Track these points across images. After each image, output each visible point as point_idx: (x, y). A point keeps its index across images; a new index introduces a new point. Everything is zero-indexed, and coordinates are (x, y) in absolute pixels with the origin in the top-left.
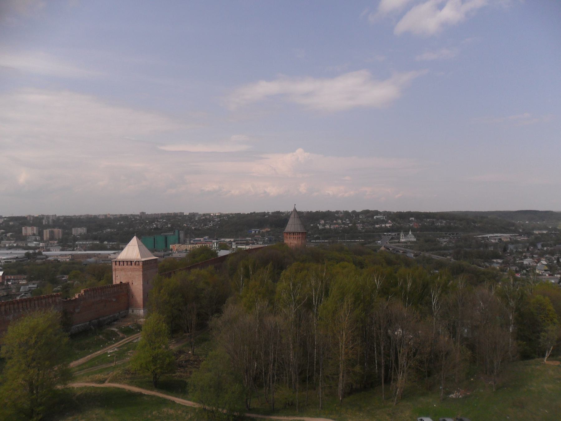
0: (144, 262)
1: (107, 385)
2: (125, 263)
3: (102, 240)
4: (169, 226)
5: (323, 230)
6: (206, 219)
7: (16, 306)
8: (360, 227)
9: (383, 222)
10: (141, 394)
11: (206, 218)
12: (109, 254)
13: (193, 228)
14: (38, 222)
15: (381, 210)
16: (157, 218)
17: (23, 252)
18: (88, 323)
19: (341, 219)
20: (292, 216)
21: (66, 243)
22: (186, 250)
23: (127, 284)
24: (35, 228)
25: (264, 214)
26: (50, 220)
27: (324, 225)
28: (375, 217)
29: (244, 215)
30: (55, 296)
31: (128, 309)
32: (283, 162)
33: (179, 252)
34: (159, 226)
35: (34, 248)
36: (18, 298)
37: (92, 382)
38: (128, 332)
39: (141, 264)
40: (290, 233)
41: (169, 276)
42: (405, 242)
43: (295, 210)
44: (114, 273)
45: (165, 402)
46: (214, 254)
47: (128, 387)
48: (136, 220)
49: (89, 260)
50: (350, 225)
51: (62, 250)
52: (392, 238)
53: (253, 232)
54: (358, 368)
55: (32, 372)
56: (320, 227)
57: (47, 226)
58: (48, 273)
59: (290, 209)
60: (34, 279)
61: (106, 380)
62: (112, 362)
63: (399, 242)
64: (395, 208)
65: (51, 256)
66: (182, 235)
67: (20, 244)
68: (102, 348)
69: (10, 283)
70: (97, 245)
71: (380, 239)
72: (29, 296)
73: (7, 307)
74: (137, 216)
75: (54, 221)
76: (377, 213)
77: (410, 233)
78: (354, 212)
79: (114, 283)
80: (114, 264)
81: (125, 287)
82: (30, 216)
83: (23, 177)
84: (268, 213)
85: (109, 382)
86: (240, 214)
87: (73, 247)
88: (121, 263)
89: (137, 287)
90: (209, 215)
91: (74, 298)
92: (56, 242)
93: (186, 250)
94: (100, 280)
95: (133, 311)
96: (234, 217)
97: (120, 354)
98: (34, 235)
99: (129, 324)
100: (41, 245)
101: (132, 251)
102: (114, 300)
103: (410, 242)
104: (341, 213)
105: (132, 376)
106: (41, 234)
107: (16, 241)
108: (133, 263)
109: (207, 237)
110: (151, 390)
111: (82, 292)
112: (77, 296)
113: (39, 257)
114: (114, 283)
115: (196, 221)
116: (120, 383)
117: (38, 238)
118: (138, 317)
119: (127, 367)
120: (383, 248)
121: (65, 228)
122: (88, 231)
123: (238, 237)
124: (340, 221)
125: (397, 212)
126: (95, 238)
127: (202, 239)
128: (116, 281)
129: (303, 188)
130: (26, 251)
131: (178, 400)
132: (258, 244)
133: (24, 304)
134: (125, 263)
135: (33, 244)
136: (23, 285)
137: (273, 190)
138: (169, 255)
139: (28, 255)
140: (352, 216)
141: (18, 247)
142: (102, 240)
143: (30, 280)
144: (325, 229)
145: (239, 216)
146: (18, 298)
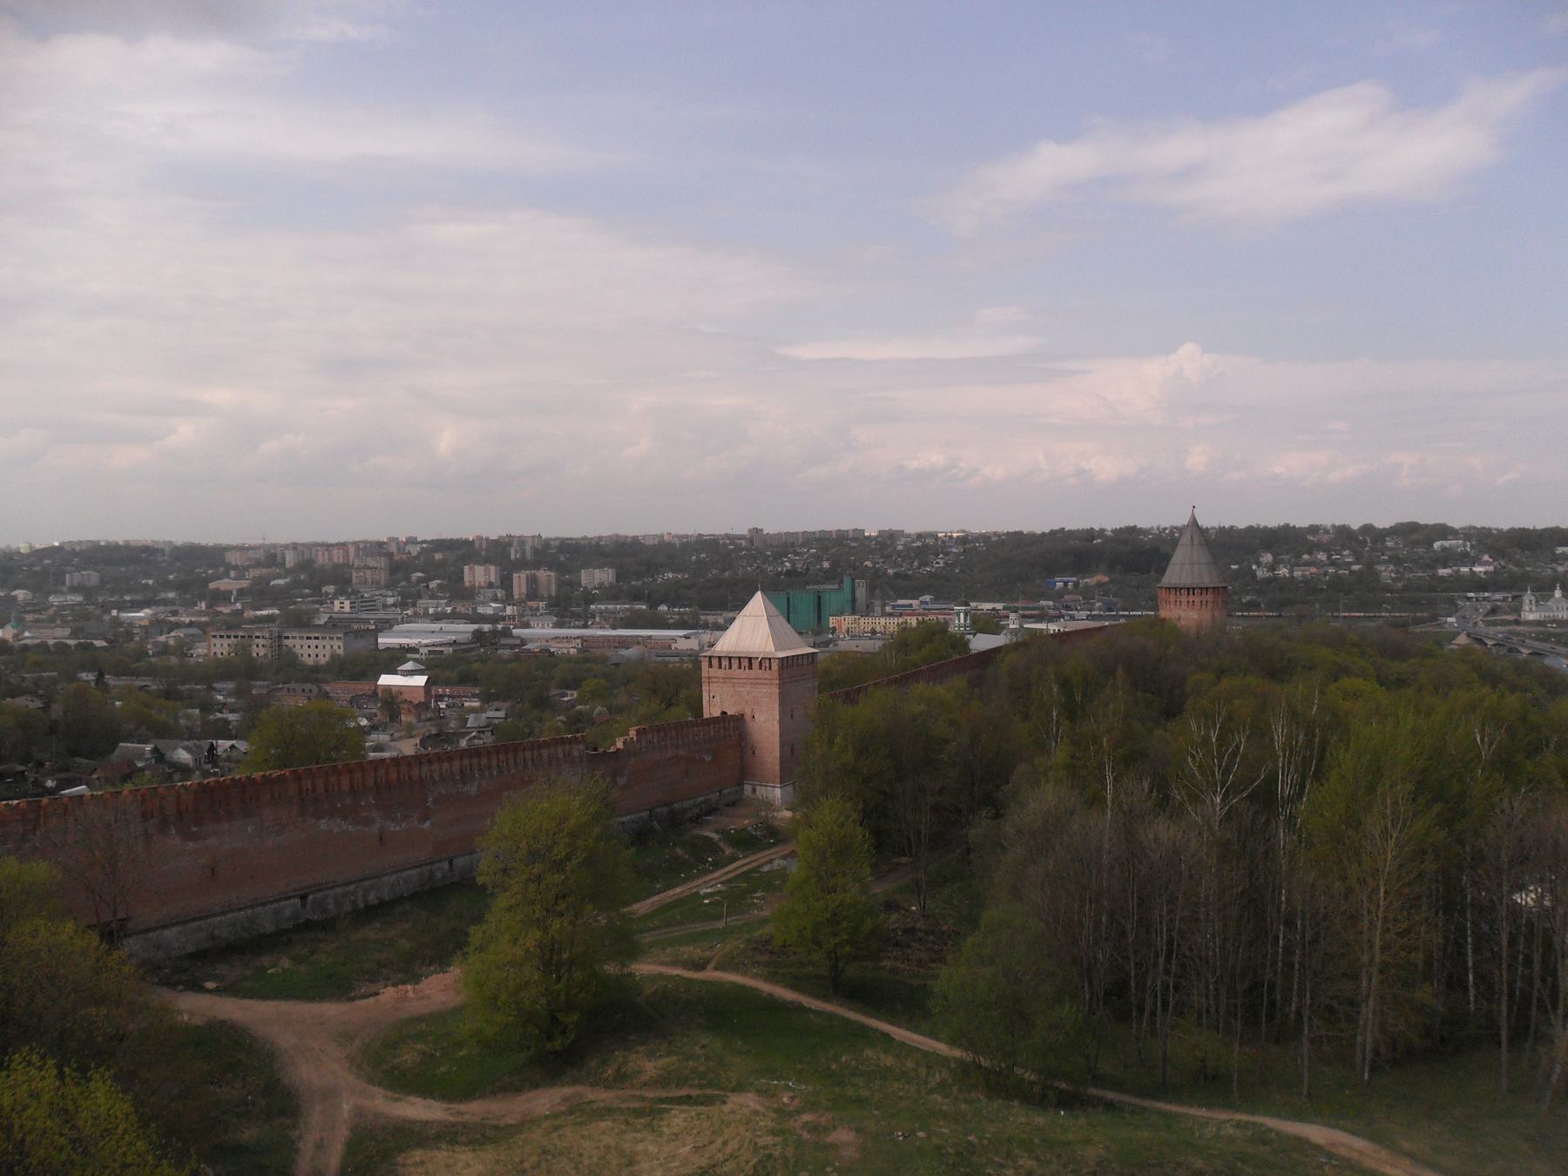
0: (786, 663)
1: (710, 974)
2: (735, 664)
3: (653, 602)
4: (826, 565)
5: (1268, 581)
6: (926, 547)
7: (484, 761)
8: (1386, 573)
9: (1464, 558)
10: (800, 1008)
11: (925, 546)
12: (674, 639)
13: (891, 571)
14: (498, 552)
15: (1456, 523)
16: (793, 545)
17: (462, 630)
18: (645, 814)
19: (1328, 551)
20: (1186, 539)
21: (567, 606)
22: (874, 632)
23: (739, 719)
24: (492, 568)
25: (1089, 535)
26: (528, 548)
27: (1272, 568)
28: (1437, 545)
29: (1032, 536)
30: (570, 741)
31: (741, 784)
32: (1134, 384)
33: (853, 637)
34: (799, 566)
35: (493, 619)
36: (463, 743)
37: (674, 964)
38: (746, 842)
39: (775, 666)
40: (1177, 589)
41: (850, 698)
42: (1538, 623)
43: (1194, 522)
44: (705, 687)
45: (862, 1033)
46: (960, 643)
47: (766, 987)
48: (739, 548)
49: (623, 652)
50: (1356, 567)
51: (558, 625)
52: (1494, 611)
53: (1060, 585)
54: (1425, 994)
55: (556, 925)
56: (1261, 573)
57: (522, 564)
58: (527, 682)
59: (1182, 520)
60: (496, 697)
61: (708, 961)
62: (718, 917)
63: (1517, 622)
64: (1503, 519)
65: (531, 640)
66: (861, 593)
67: (460, 609)
68: (684, 881)
69: (443, 706)
70: (640, 613)
71: (1453, 609)
72: (488, 739)
73: (466, 762)
74: (741, 537)
75: (536, 551)
76: (1443, 531)
77: (1558, 594)
78: (1367, 529)
79: (706, 715)
80: (705, 665)
81: (734, 727)
82: (480, 538)
83: (447, 439)
84: (1102, 531)
85: (716, 969)
86: (1020, 533)
87: (585, 619)
88: (725, 663)
89: (766, 725)
90: (934, 536)
91: (612, 749)
92: (542, 604)
93: (874, 632)
94: (669, 705)
95: (754, 790)
96: (1002, 543)
97: (735, 898)
98: (491, 585)
99: (742, 822)
100: (509, 610)
101: (753, 630)
102: (708, 758)
103: (1554, 621)
104: (1326, 531)
105: (770, 957)
106: (506, 583)
107: (451, 600)
108: (756, 664)
109: (927, 598)
110: (825, 998)
111: (632, 733)
112: (620, 745)
113: (504, 641)
114: (706, 715)
115: (899, 554)
116: (745, 974)
117: (500, 593)
118: (768, 805)
119: (757, 934)
120: (1462, 640)
121: (564, 570)
122: (619, 577)
123: (1016, 600)
124: (1322, 556)
125: (1513, 530)
126: (636, 596)
127: (915, 603)
128: (711, 710)
129: (1197, 459)
130: (476, 626)
131: (899, 1033)
132: (1072, 618)
133: (511, 755)
134: (735, 664)
135: (489, 609)
136: (473, 710)
137: (1106, 466)
138: (827, 643)
139: (478, 635)
140: (1363, 541)
141: (455, 617)
142: (653, 602)
143: (487, 699)
144: (1275, 579)
145: (1018, 540)
146: (463, 743)
